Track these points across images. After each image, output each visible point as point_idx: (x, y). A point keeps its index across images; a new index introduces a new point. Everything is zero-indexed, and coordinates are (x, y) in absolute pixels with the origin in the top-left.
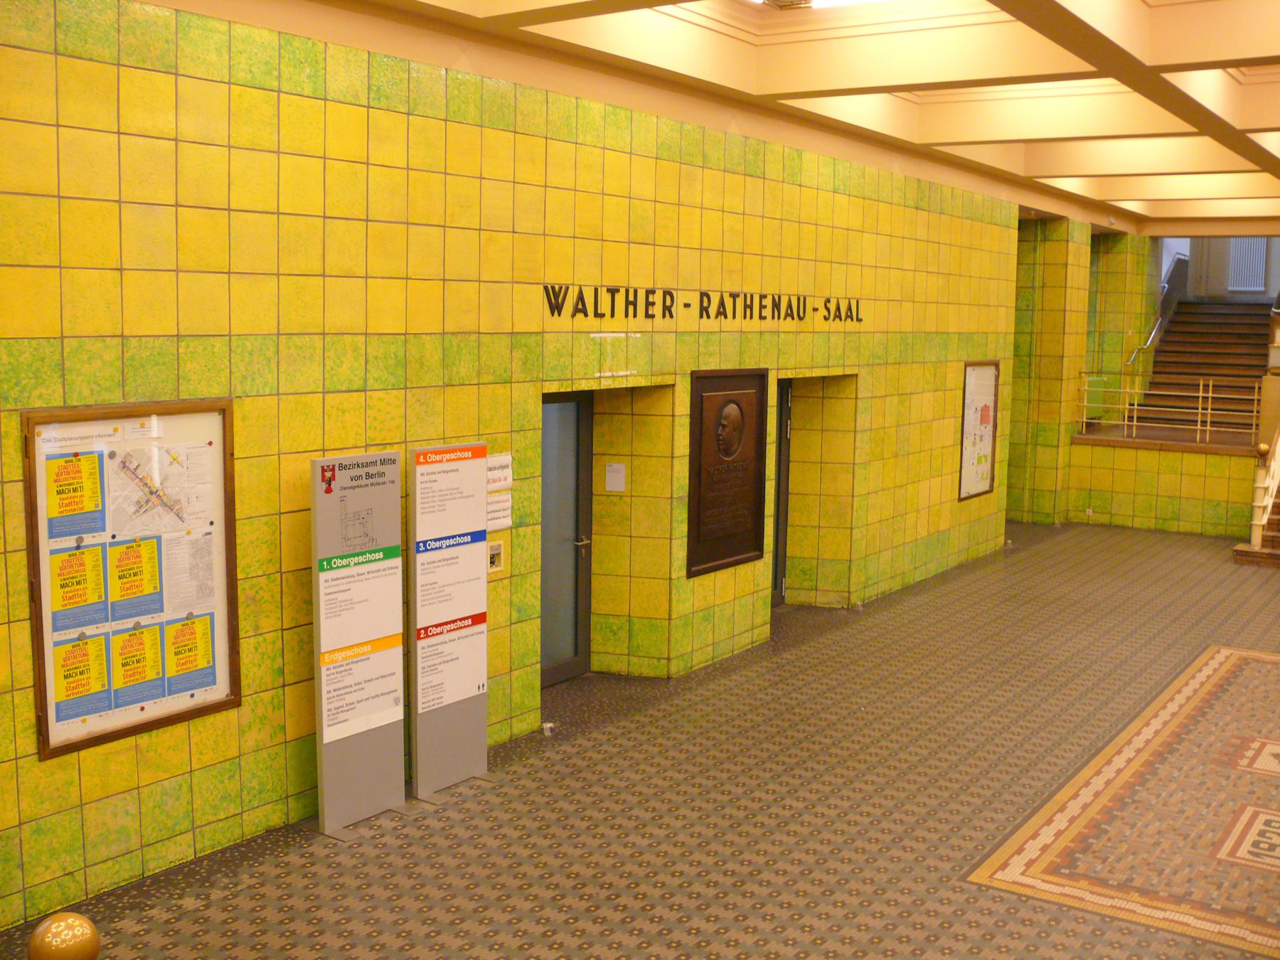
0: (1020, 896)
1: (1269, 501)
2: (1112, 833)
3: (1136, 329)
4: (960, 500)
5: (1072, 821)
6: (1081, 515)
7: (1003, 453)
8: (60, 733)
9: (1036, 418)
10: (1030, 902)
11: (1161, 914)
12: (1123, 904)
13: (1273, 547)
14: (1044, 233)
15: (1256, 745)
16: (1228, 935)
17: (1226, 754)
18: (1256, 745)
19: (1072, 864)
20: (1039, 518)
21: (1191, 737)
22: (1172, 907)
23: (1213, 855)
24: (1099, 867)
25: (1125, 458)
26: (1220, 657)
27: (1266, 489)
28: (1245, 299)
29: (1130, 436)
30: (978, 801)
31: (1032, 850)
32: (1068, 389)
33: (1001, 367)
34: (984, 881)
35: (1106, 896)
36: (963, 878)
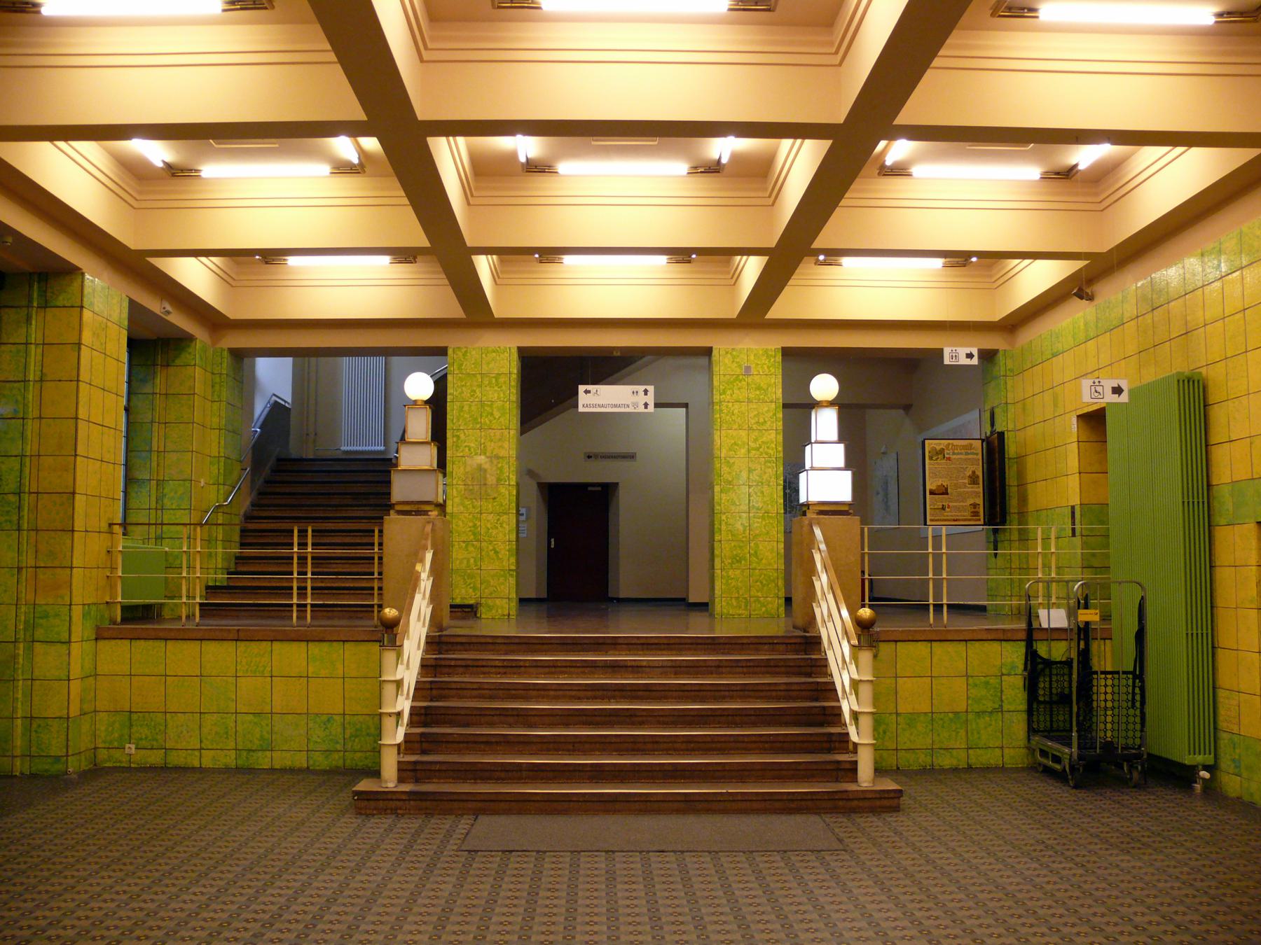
1: (404, 705)
3: (204, 468)
6: (117, 754)
9: (31, 597)
13: (417, 781)
14: (43, 293)
20: (40, 766)
25: (182, 656)
32: (87, 550)
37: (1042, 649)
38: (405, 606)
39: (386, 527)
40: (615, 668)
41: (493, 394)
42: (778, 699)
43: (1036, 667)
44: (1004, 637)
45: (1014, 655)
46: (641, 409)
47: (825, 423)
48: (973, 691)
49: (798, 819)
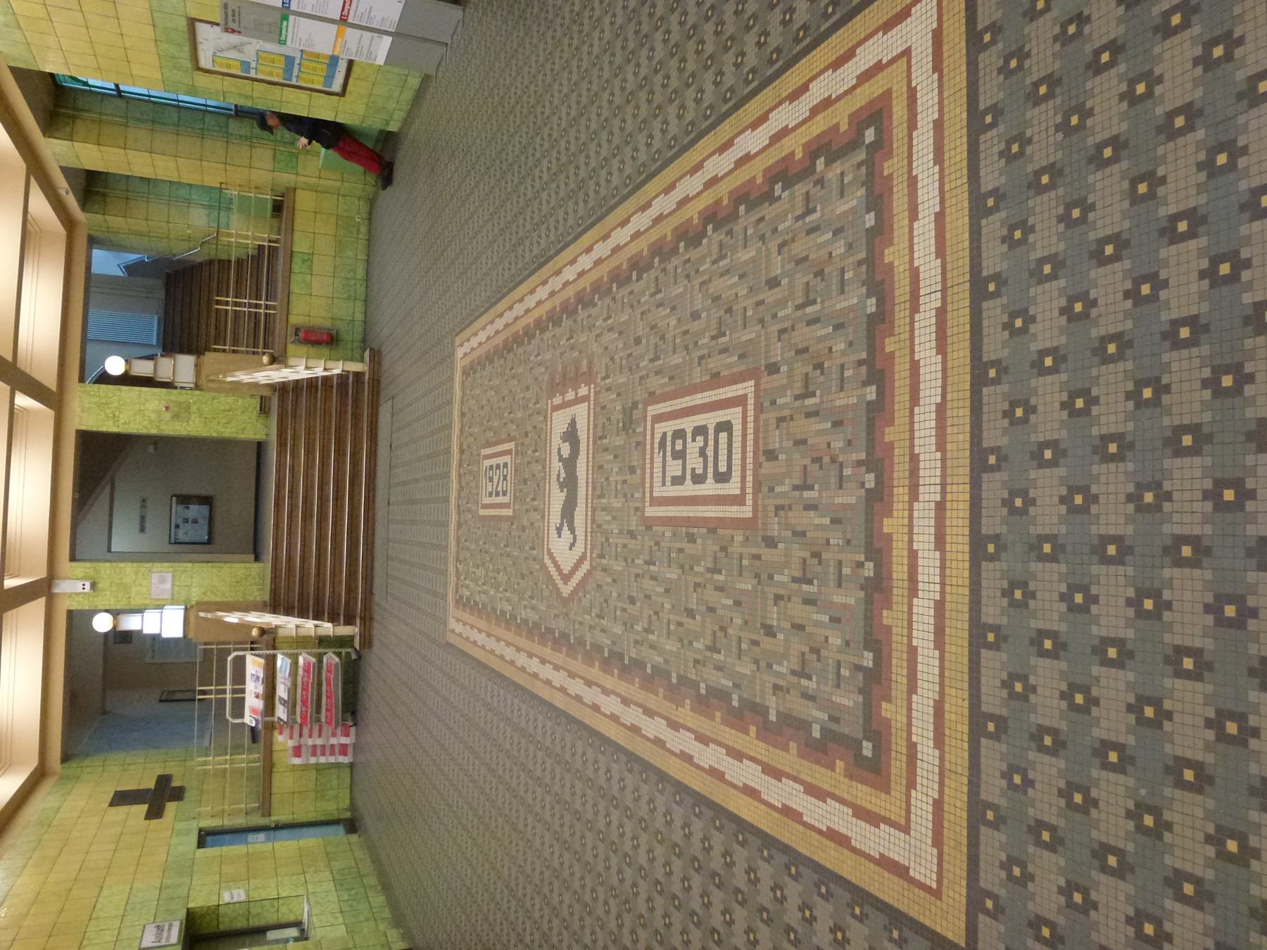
4: (192, 22)
8: (337, 86)
18: (583, 391)
26: (459, 628)
27: (297, 627)
38: (248, 627)
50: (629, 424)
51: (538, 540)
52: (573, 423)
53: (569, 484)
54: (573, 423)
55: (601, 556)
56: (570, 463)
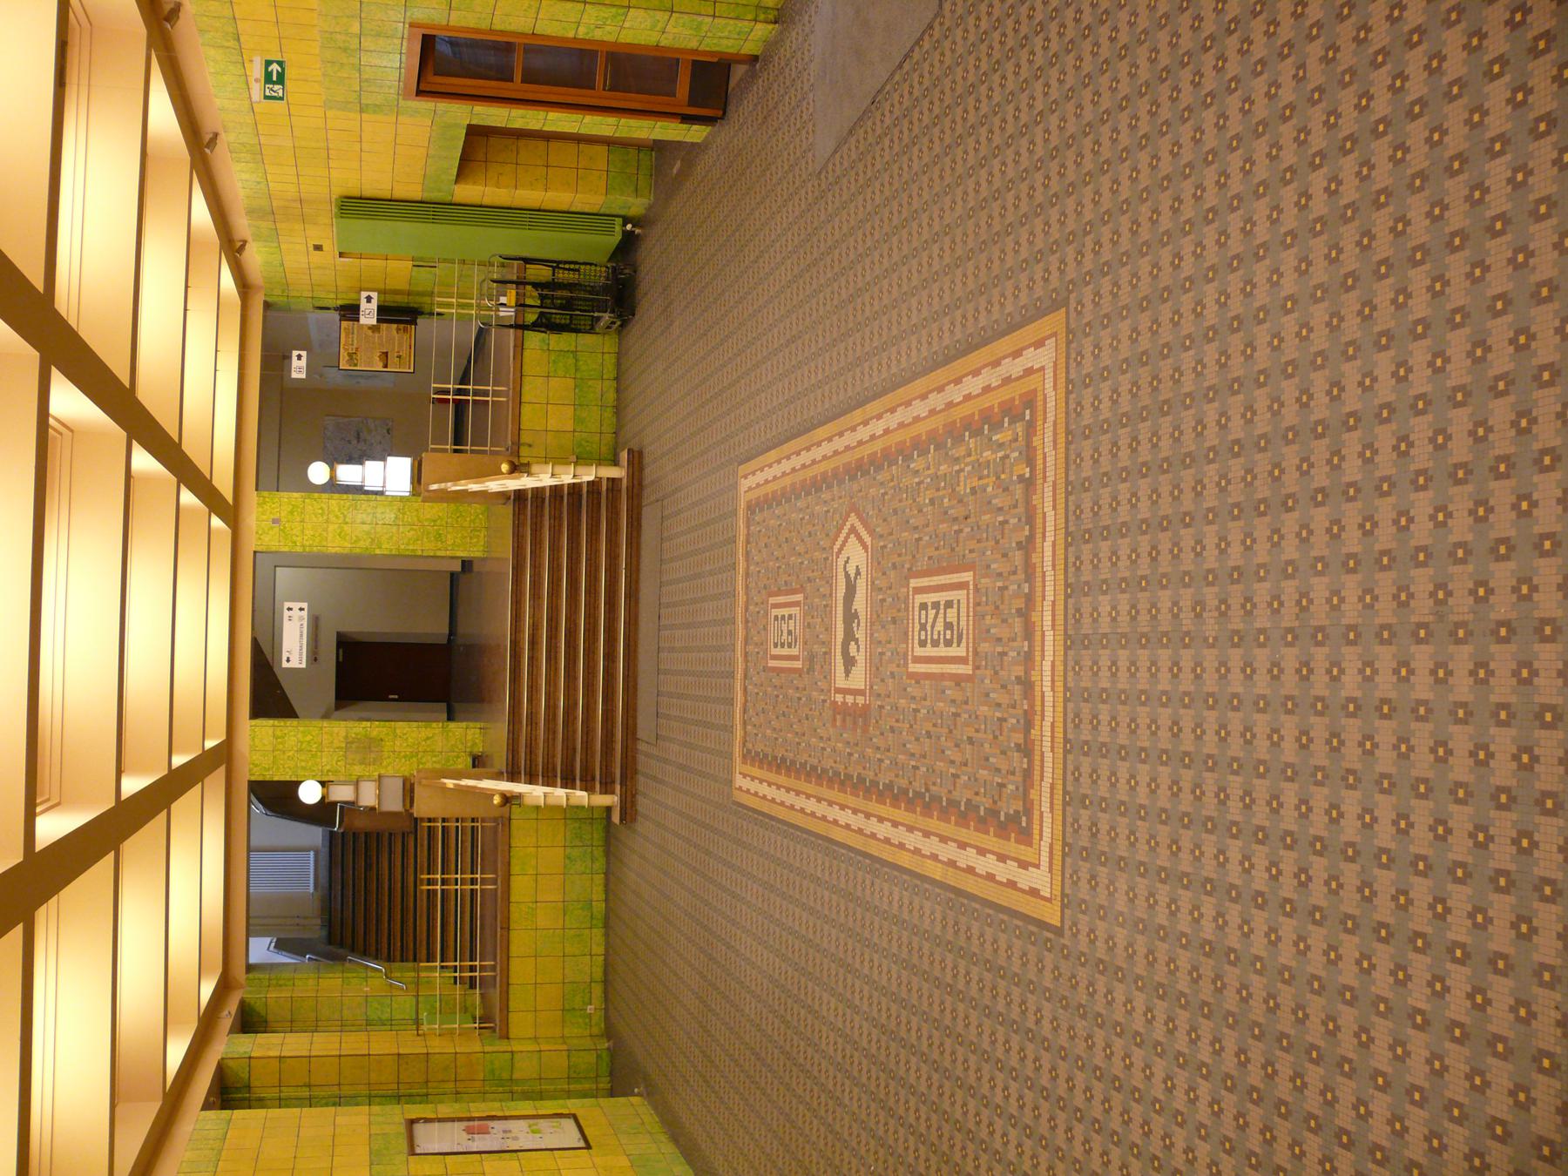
0: (1064, 855)
2: (968, 794)
3: (364, 984)
4: (588, 1147)
5: (963, 846)
6: (595, 1019)
7: (526, 1107)
9: (478, 1084)
10: (1069, 840)
11: (1048, 755)
12: (1047, 744)
15: (839, 698)
16: (1053, 620)
17: (855, 723)
18: (839, 698)
19: (1014, 818)
21: (841, 768)
22: (1037, 689)
23: (969, 678)
24: (1011, 787)
25: (521, 971)
28: (324, 873)
29: (493, 968)
30: (959, 1137)
31: (1004, 871)
33: (414, 1116)
34: (1057, 905)
35: (1042, 761)
36: (1059, 932)
37: (531, 317)
38: (487, 795)
39: (422, 815)
40: (534, 643)
41: (291, 741)
42: (561, 525)
43: (545, 325)
44: (520, 347)
45: (534, 339)
46: (305, 613)
47: (348, 474)
48: (560, 373)
49: (644, 523)
50: (811, 658)
51: (877, 559)
52: (847, 672)
53: (850, 617)
54: (847, 672)
55: (826, 559)
56: (849, 636)
